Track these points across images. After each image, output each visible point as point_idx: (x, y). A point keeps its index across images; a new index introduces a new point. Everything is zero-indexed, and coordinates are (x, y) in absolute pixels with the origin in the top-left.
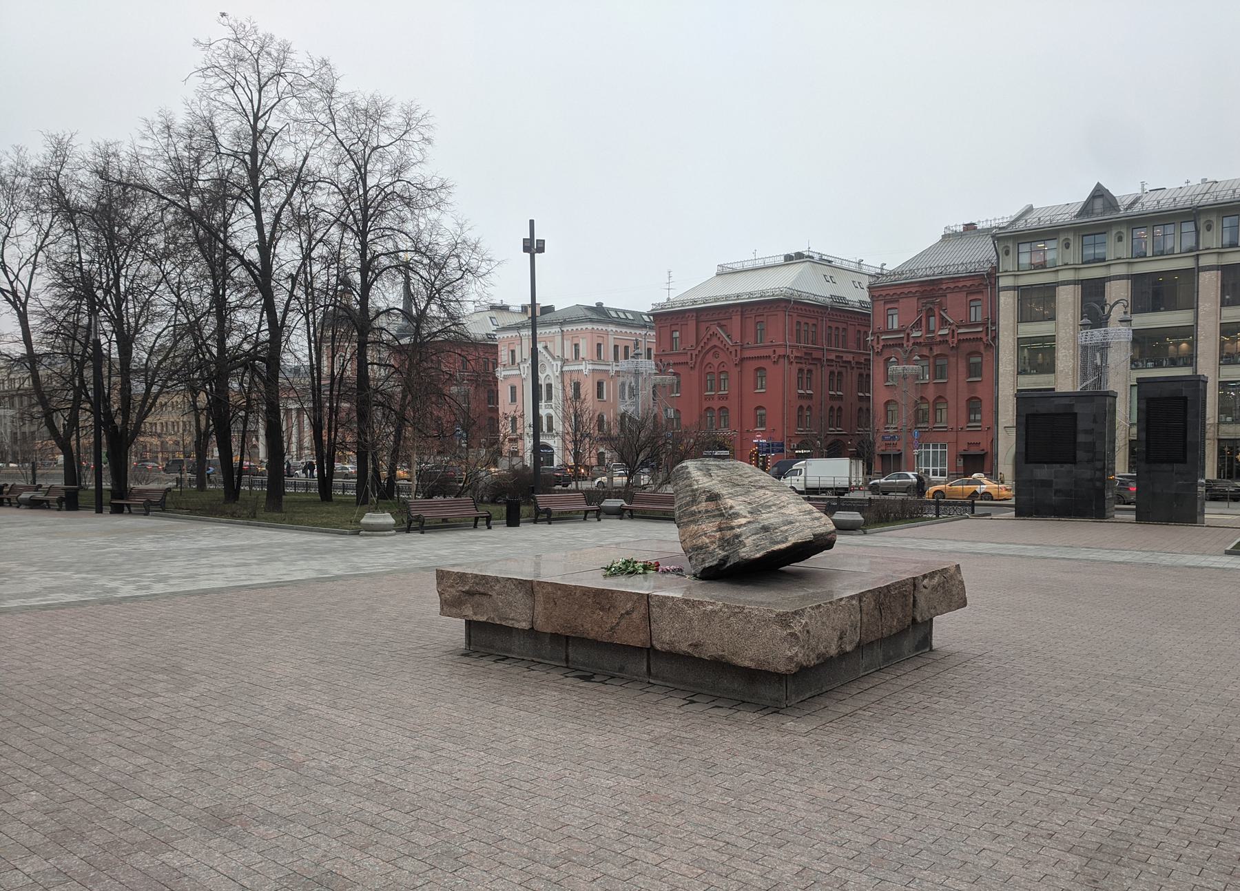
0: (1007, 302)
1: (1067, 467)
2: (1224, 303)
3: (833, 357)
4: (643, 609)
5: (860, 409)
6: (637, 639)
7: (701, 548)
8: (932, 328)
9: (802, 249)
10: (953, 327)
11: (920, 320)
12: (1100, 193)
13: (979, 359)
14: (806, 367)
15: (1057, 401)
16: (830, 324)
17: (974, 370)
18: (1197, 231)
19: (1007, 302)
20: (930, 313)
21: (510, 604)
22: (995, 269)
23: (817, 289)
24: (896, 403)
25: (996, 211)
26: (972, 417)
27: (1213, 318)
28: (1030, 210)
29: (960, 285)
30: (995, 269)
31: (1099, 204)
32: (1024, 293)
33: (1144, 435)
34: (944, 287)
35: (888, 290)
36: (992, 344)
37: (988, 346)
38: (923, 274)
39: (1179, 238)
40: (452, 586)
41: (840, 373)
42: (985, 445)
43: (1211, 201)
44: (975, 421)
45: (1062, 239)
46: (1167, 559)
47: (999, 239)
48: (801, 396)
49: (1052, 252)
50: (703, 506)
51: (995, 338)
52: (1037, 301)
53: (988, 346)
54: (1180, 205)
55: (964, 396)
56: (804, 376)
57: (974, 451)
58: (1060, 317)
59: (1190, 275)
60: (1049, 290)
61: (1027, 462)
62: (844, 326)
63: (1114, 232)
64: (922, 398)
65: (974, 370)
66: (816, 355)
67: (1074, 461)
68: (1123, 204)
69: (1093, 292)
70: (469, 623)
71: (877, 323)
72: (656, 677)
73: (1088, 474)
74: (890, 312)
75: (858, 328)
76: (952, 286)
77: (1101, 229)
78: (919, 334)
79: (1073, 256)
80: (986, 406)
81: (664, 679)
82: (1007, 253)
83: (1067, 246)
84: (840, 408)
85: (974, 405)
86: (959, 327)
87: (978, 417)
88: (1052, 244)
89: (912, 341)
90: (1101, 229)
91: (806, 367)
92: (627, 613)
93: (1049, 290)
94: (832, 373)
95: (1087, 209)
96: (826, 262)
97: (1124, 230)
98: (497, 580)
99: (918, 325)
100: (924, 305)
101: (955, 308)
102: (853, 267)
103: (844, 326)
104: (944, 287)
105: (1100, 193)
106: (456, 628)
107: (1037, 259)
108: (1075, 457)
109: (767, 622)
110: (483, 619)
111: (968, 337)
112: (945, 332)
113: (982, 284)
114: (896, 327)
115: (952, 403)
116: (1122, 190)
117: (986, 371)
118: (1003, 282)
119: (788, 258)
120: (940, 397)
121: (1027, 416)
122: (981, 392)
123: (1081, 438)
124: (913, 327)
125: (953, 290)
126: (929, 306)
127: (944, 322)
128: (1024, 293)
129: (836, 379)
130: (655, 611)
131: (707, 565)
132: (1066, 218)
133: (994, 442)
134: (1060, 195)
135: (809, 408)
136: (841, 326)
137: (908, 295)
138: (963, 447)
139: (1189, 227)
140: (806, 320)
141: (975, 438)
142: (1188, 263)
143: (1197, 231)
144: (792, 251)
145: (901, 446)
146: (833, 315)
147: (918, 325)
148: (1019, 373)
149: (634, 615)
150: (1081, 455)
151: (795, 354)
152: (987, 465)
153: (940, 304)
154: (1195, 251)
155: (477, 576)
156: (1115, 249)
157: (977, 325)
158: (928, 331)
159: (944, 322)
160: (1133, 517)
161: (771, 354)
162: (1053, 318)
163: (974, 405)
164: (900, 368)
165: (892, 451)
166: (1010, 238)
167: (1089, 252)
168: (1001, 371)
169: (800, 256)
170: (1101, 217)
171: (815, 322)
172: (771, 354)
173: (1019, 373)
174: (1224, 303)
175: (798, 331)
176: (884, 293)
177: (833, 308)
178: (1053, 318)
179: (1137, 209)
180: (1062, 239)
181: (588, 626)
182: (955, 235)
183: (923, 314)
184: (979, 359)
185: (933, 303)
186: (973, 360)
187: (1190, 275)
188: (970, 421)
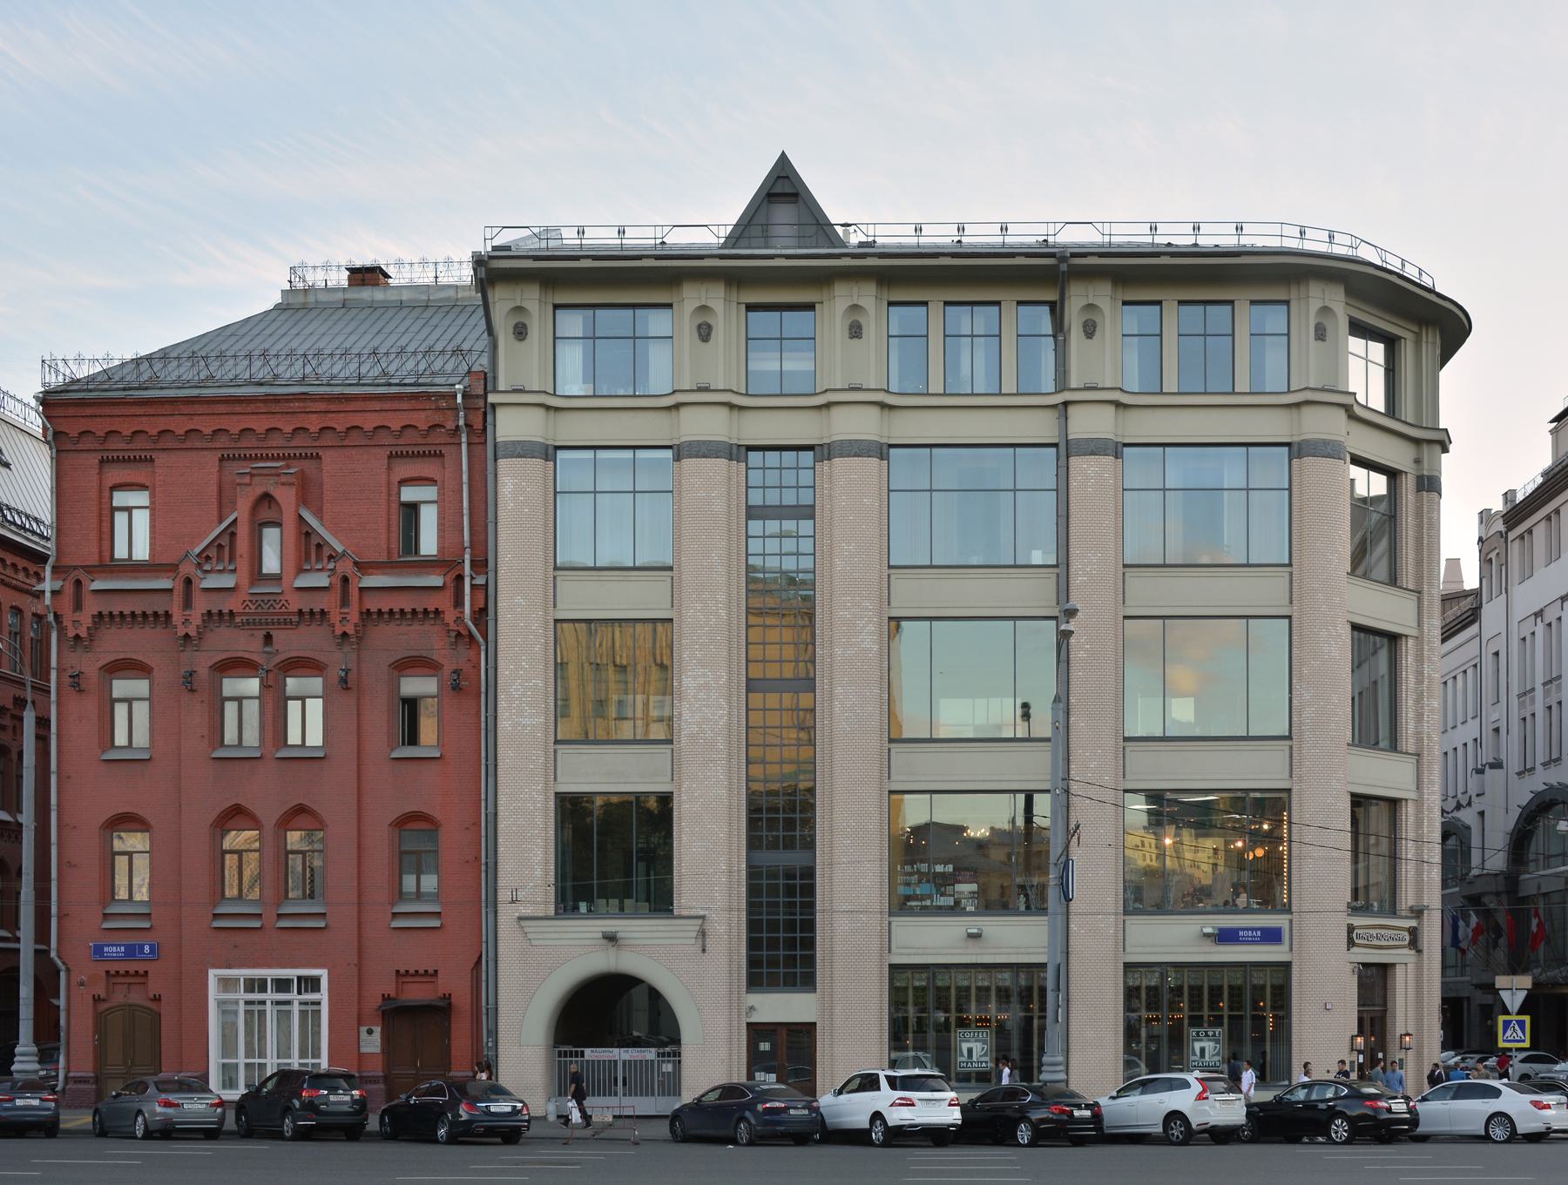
2: (901, 905)
10: (345, 567)
11: (231, 533)
18: (1059, 327)
26: (409, 882)
29: (369, 422)
37: (463, 638)
38: (235, 374)
42: (454, 983)
44: (419, 895)
46: (1411, 569)
57: (416, 994)
78: (228, 581)
82: (521, 332)
83: (705, 332)
86: (363, 567)
95: (751, 225)
99: (223, 548)
105: (783, 189)
112: (322, 580)
114: (142, 552)
118: (510, 426)
120: (300, 810)
124: (204, 557)
133: (481, 968)
174: (901, 905)
183: (241, 512)
188: (401, 896)
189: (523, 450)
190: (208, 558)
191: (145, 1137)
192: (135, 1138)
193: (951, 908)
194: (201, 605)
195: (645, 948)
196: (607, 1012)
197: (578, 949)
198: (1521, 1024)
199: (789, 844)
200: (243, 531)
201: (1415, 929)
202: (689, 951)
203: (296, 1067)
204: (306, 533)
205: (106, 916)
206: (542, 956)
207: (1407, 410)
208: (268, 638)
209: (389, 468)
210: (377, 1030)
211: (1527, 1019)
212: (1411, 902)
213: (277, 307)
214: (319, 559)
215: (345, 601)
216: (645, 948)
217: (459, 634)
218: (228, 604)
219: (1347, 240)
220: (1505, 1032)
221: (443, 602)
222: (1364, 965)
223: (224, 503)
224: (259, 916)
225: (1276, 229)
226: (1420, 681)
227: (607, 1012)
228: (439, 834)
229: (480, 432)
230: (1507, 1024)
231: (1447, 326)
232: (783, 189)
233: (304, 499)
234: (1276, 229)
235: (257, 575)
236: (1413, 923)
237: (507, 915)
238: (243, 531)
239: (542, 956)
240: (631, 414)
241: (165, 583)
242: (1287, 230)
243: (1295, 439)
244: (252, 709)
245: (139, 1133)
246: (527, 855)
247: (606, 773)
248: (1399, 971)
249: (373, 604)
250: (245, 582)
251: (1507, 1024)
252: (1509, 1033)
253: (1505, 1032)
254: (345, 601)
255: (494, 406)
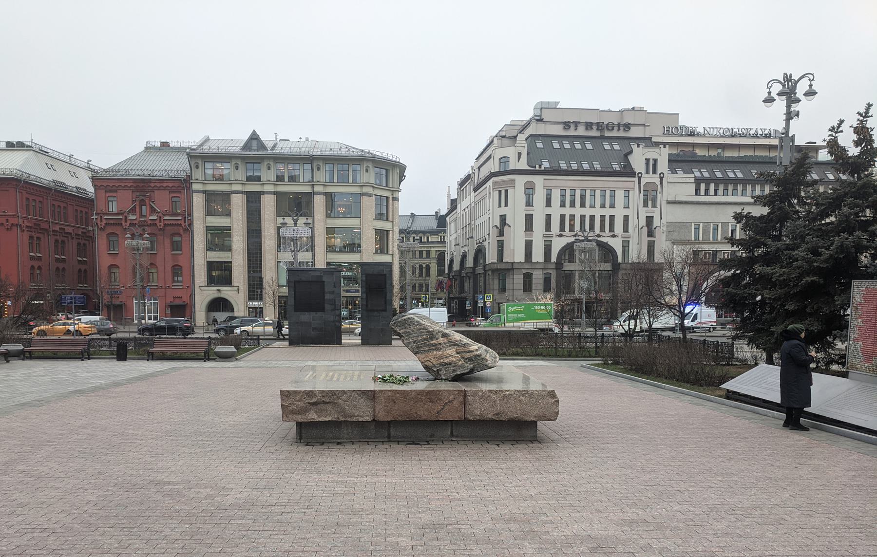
0: (198, 201)
1: (319, 314)
3: (57, 228)
4: (461, 399)
5: (80, 270)
6: (456, 416)
7: (450, 364)
8: (144, 214)
9: (26, 140)
11: (135, 207)
12: (254, 137)
13: (179, 239)
14: (60, 239)
15: (313, 274)
16: (54, 202)
17: (176, 246)
18: (312, 170)
19: (198, 201)
20: (142, 203)
21: (355, 406)
22: (190, 177)
23: (39, 172)
24: (118, 267)
25: (187, 136)
26: (176, 279)
27: (322, 224)
28: (207, 140)
29: (165, 185)
30: (190, 177)
31: (254, 144)
32: (210, 196)
33: (365, 295)
34: (152, 185)
35: (107, 183)
36: (189, 229)
37: (186, 230)
39: (304, 172)
40: (300, 400)
41: (63, 242)
42: (186, 299)
43: (319, 153)
44: (178, 281)
45: (234, 163)
47: (191, 157)
48: (32, 258)
49: (226, 169)
50: (441, 340)
51: (191, 224)
52: (218, 202)
53: (186, 230)
54: (302, 153)
55: (169, 265)
56: (35, 242)
57: (178, 302)
58: (234, 214)
59: (310, 196)
60: (226, 196)
61: (295, 311)
62: (65, 205)
63: (266, 163)
64: (151, 264)
65: (176, 246)
66: (43, 226)
67: (323, 310)
68: (269, 145)
69: (253, 200)
70: (300, 425)
71: (100, 206)
72: (457, 436)
73: (332, 318)
74: (110, 199)
75: (76, 207)
76: (158, 185)
77: (259, 160)
78: (134, 217)
79: (241, 175)
80: (185, 271)
81: (462, 437)
82: (197, 167)
83: (237, 168)
84: (64, 269)
85: (176, 270)
86: (164, 215)
87: (180, 279)
88: (227, 165)
89: (129, 222)
90: (259, 160)
91: (35, 235)
92: (450, 402)
93: (226, 196)
94: (56, 241)
95: (247, 146)
96: (42, 152)
97: (271, 163)
98: (344, 392)
100: (138, 196)
101: (162, 201)
102: (67, 159)
103: (65, 205)
104: (152, 185)
105: (254, 137)
106: (290, 426)
107: (218, 173)
108: (324, 308)
109: (543, 397)
110: (329, 419)
111: (171, 222)
112: (155, 217)
113: (180, 186)
115: (161, 268)
116: (266, 137)
117: (185, 246)
118: (195, 187)
119: (10, 145)
121: (295, 282)
122: (182, 262)
123: (327, 296)
124: (129, 212)
125: (159, 189)
126: (141, 198)
127: (153, 211)
128: (210, 196)
129: (60, 246)
130: (470, 399)
131: (459, 373)
132: (236, 149)
133: (192, 296)
134: (230, 135)
135: (39, 268)
136: (63, 205)
137: (125, 188)
138: (169, 300)
139: (308, 167)
140: (34, 197)
141: (178, 293)
142: (308, 189)
143: (312, 170)
144: (14, 140)
145: (122, 298)
146: (55, 196)
147: (133, 211)
148: (207, 250)
149: (455, 402)
150: (328, 307)
151: (26, 223)
152: (188, 312)
153: (150, 197)
154: (312, 183)
155: (323, 391)
156: (268, 175)
157: (178, 215)
158: (141, 216)
159: (153, 211)
160: (287, 343)
161: (4, 222)
162: (229, 215)
163: (176, 270)
164: (134, 242)
165: (116, 302)
166: (199, 157)
167: (250, 174)
168: (195, 247)
169: (21, 145)
170: (254, 154)
171: (41, 199)
172: (4, 222)
173: (207, 250)
175: (28, 205)
176: (105, 184)
177: (56, 190)
178: (229, 215)
179: (278, 150)
180: (234, 163)
181: (421, 413)
182: (154, 148)
184: (179, 239)
185: (144, 196)
186: (176, 239)
187: (310, 196)
188: (174, 281)
189: (198, 192)
193: (82, 353)
195: (226, 292)
196: (219, 305)
197: (212, 292)
199: (257, 272)
200: (138, 207)
202: (237, 294)
203: (320, 264)
204: (152, 207)
206: (203, 295)
216: (226, 292)
221: (182, 222)
223: (133, 202)
224: (500, 192)
227: (219, 305)
228: (180, 271)
229: (189, 188)
231: (399, 169)
233: (150, 200)
235: (141, 216)
238: (138, 207)
239: (203, 295)
246: (201, 276)
247: (217, 256)
249: (166, 222)
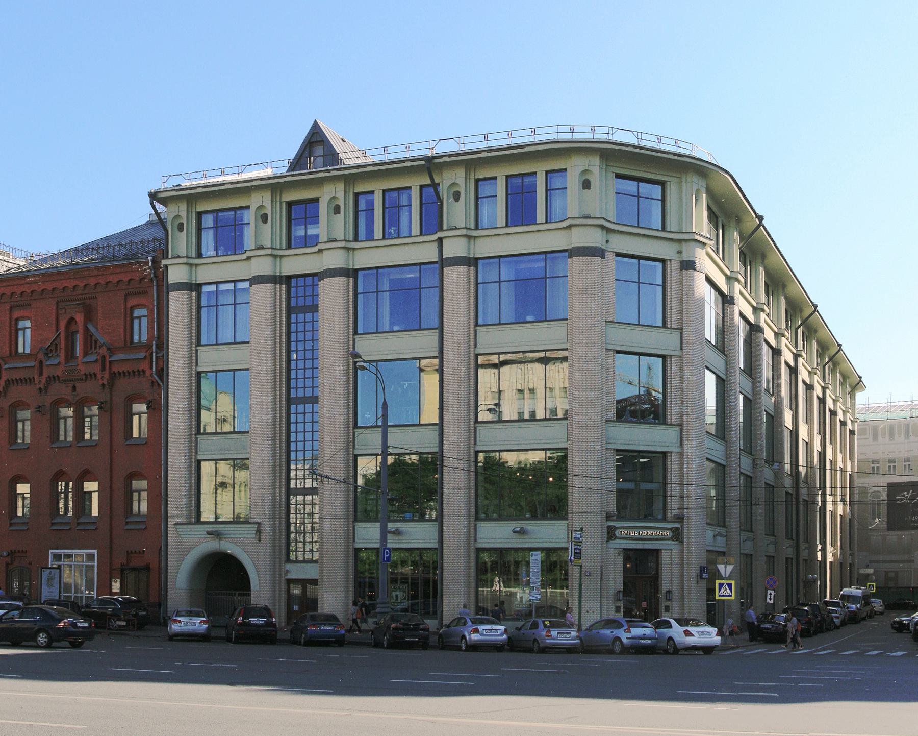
10: (103, 351)
105: (316, 140)
133: (162, 550)
189: (179, 287)
190: (51, 351)
191: (465, 650)
192: (461, 650)
194: (46, 372)
198: (730, 585)
201: (677, 528)
205: (78, 524)
207: (672, 225)
208: (74, 388)
209: (126, 301)
210: (119, 581)
211: (733, 582)
212: (675, 512)
213: (147, 224)
214: (96, 348)
215: (41, 373)
217: (153, 382)
218: (59, 372)
219: (605, 130)
220: (720, 590)
222: (624, 549)
225: (555, 129)
226: (681, 382)
230: (721, 585)
232: (316, 140)
234: (555, 129)
236: (677, 525)
237: (171, 522)
240: (232, 264)
241: (32, 364)
242: (561, 129)
243: (570, 247)
244: (70, 422)
245: (464, 648)
248: (665, 555)
249: (116, 369)
250: (63, 362)
251: (721, 585)
252: (722, 591)
253: (720, 590)
254: (103, 369)
255: (166, 267)
